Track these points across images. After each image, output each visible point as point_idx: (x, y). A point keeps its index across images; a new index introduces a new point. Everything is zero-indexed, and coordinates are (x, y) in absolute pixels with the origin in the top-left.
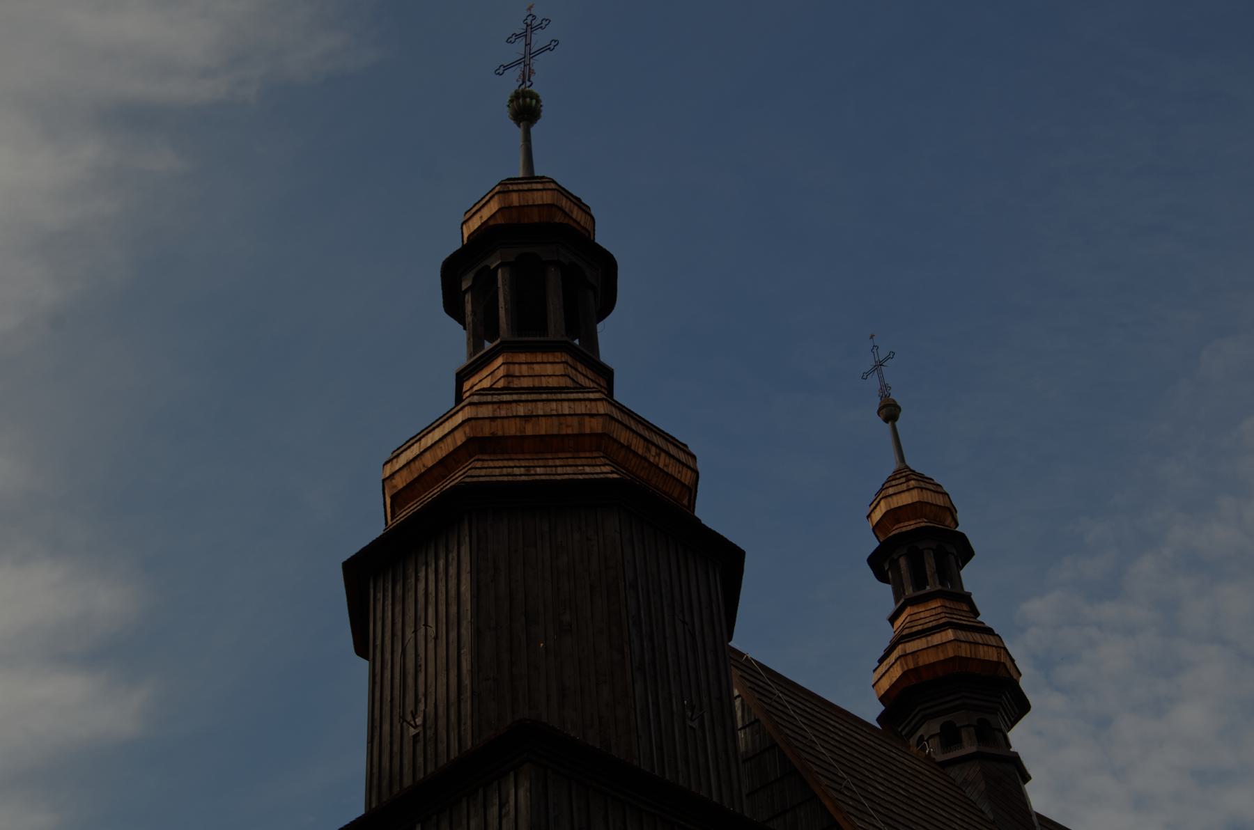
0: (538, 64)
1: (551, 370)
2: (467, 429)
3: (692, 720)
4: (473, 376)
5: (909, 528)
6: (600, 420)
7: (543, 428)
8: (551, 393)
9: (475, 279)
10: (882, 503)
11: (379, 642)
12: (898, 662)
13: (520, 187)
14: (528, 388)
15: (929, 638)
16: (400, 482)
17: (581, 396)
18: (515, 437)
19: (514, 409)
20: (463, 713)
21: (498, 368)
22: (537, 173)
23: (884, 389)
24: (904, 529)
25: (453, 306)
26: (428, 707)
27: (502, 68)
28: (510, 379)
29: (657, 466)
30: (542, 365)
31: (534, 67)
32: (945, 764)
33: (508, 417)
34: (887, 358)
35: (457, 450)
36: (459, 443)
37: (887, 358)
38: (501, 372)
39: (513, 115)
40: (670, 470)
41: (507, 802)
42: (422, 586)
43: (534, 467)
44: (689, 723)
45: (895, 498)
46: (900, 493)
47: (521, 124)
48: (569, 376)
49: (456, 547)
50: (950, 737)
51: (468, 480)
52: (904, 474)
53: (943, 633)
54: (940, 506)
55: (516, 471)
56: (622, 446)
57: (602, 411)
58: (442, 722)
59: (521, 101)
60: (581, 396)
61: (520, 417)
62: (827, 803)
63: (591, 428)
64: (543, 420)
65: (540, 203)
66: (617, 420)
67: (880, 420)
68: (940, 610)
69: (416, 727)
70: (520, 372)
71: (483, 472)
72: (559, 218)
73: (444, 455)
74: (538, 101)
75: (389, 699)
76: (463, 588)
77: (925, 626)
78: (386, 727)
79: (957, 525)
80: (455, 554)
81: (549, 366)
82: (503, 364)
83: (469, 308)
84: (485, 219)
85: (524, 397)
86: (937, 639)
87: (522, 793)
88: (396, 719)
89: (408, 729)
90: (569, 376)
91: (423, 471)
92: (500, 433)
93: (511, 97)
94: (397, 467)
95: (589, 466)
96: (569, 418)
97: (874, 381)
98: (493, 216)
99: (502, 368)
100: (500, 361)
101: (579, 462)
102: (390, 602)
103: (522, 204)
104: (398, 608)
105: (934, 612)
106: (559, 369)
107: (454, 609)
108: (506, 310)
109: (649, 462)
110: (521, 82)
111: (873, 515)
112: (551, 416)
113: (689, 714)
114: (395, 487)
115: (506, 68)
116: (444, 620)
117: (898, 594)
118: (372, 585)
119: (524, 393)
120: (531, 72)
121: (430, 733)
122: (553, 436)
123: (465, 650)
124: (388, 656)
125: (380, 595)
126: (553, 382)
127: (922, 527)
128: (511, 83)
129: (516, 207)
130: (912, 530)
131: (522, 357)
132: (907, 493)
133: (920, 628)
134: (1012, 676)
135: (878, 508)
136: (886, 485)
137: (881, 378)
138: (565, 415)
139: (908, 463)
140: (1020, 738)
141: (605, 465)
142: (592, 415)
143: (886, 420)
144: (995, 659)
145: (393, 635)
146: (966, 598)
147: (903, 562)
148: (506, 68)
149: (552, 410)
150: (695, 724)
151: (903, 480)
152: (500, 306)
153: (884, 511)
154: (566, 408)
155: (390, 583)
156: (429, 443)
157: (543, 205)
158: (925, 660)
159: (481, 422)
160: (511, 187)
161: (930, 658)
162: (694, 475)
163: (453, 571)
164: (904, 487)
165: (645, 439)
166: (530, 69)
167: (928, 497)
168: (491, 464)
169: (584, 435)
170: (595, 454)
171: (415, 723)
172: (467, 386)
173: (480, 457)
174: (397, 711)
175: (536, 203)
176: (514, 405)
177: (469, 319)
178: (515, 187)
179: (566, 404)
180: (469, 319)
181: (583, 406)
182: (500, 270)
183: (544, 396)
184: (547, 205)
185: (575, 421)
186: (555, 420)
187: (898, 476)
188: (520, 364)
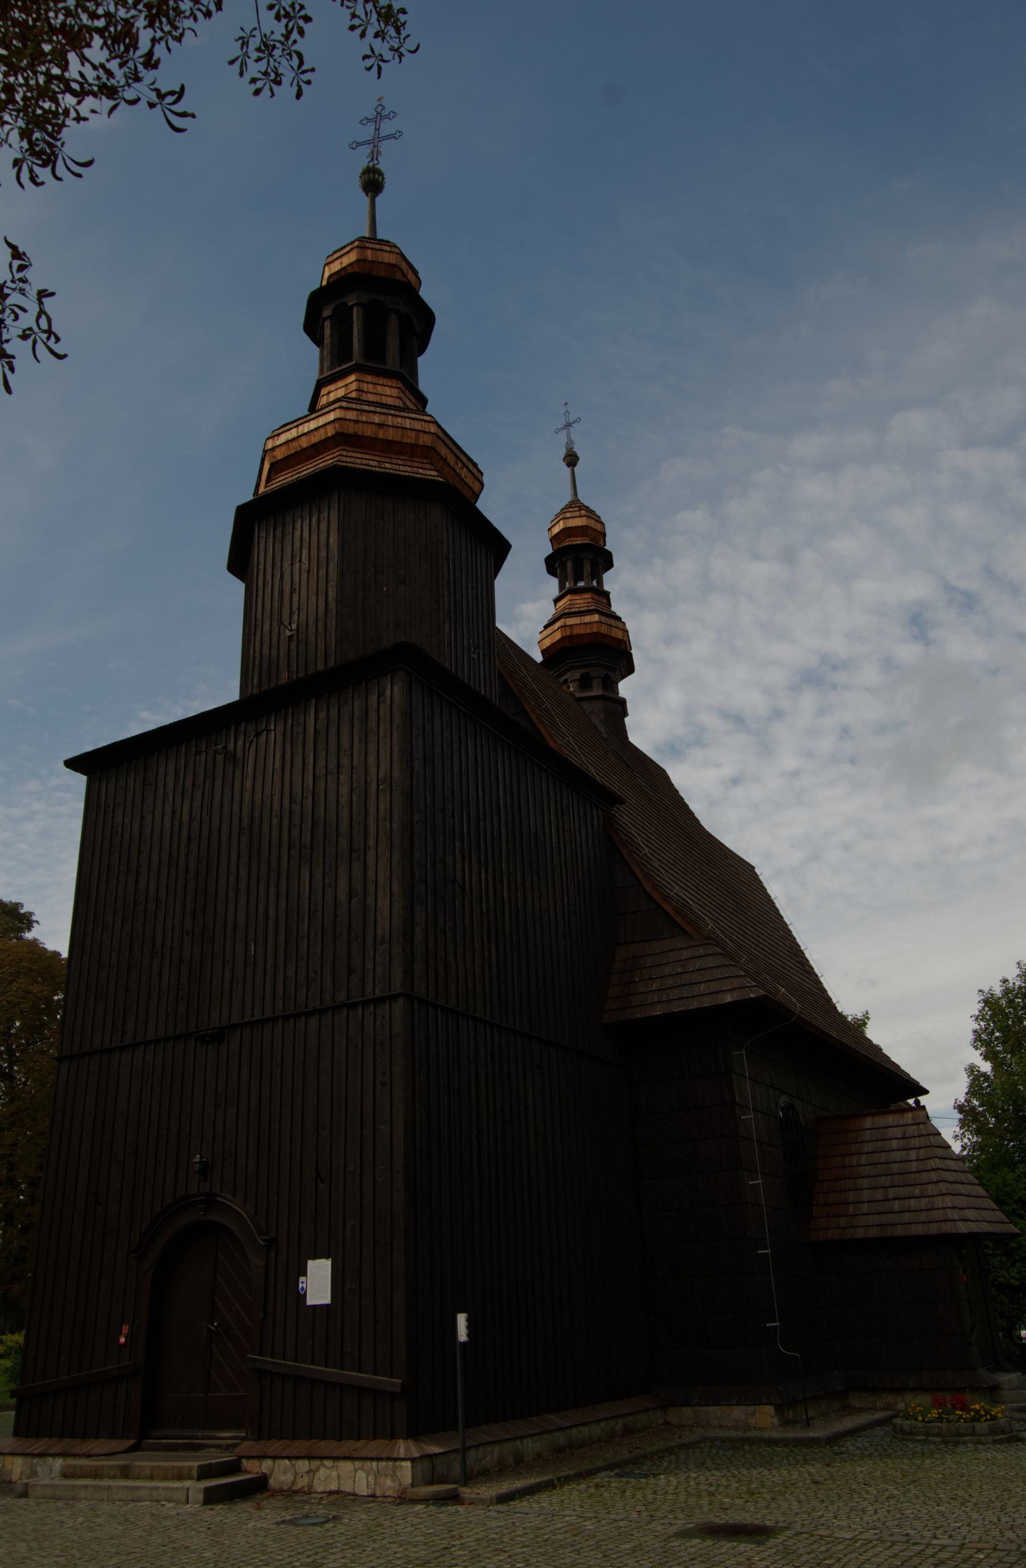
0: (385, 147)
1: (389, 392)
2: (337, 425)
3: (474, 654)
4: (330, 384)
5: (577, 542)
6: (431, 437)
7: (391, 435)
8: (397, 410)
9: (334, 311)
10: (561, 522)
11: (261, 567)
12: (560, 630)
13: (374, 246)
14: (372, 402)
15: (582, 618)
16: (279, 454)
17: (418, 417)
18: (370, 438)
19: (372, 417)
20: (328, 626)
21: (351, 383)
22: (379, 237)
23: (570, 443)
24: (574, 543)
25: (312, 327)
26: (301, 618)
27: (355, 144)
28: (360, 393)
29: (460, 476)
30: (383, 387)
31: (381, 150)
32: (580, 699)
33: (367, 423)
34: (574, 422)
35: (327, 439)
36: (330, 435)
37: (574, 422)
38: (354, 386)
39: (363, 185)
40: (468, 480)
41: (384, 693)
42: (298, 533)
43: (384, 462)
44: (472, 655)
45: (570, 520)
46: (574, 517)
47: (369, 194)
48: (401, 399)
49: (327, 510)
50: (585, 683)
51: (340, 463)
52: (575, 505)
53: (592, 616)
54: (598, 531)
55: (371, 463)
56: (442, 458)
57: (432, 431)
58: (312, 630)
59: (371, 175)
60: (418, 417)
61: (376, 424)
62: (534, 717)
63: (424, 442)
64: (391, 430)
65: (387, 262)
66: (441, 439)
67: (564, 465)
68: (590, 600)
69: (291, 630)
70: (368, 389)
71: (349, 460)
72: (399, 276)
73: (317, 441)
74: (383, 178)
75: (269, 608)
76: (331, 540)
77: (580, 609)
78: (267, 627)
79: (605, 545)
80: (326, 515)
81: (388, 388)
82: (356, 380)
83: (327, 332)
84: (344, 265)
85: (378, 410)
86: (587, 619)
87: (396, 689)
88: (275, 623)
89: (284, 631)
90: (401, 399)
91: (298, 449)
92: (360, 433)
93: (364, 170)
94: (278, 443)
95: (421, 468)
96: (409, 432)
97: (562, 438)
98: (351, 265)
99: (354, 383)
100: (352, 378)
101: (414, 464)
102: (272, 540)
103: (374, 259)
104: (278, 546)
105: (586, 601)
106: (395, 392)
107: (323, 554)
108: (359, 340)
109: (456, 472)
110: (370, 159)
111: (553, 529)
112: (398, 427)
113: (473, 649)
114: (275, 457)
115: (359, 144)
116: (316, 561)
117: (562, 586)
118: (256, 526)
119: (378, 407)
120: (379, 153)
121: (302, 636)
122: (397, 442)
123: (331, 583)
124: (269, 577)
125: (263, 534)
126: (390, 401)
127: (586, 543)
128: (361, 160)
129: (369, 261)
130: (580, 544)
131: (369, 378)
132: (579, 519)
133: (577, 610)
134: (627, 649)
135: (558, 525)
136: (564, 511)
137: (569, 435)
138: (407, 429)
139: (579, 497)
140: (625, 688)
141: (432, 470)
142: (425, 432)
143: (568, 465)
144: (621, 638)
145: (273, 564)
146: (606, 595)
147: (569, 564)
148: (359, 144)
149: (398, 423)
150: (475, 656)
151: (577, 509)
152: (354, 336)
153: (561, 527)
154: (407, 424)
155: (272, 526)
156: (306, 431)
157: (389, 264)
158: (578, 631)
159: (348, 422)
160: (367, 245)
161: (581, 631)
162: (481, 486)
163: (323, 526)
164: (578, 514)
165: (456, 456)
166: (378, 150)
167: (592, 523)
168: (353, 454)
169: (418, 446)
170: (424, 461)
171: (291, 627)
172: (324, 391)
173: (345, 448)
174: (276, 617)
175: (384, 261)
176: (372, 414)
177: (327, 340)
178: (370, 245)
179: (408, 421)
180: (327, 340)
181: (420, 425)
182: (355, 309)
183: (393, 412)
184: (393, 265)
185: (413, 434)
186: (400, 431)
187: (573, 506)
188: (368, 383)
